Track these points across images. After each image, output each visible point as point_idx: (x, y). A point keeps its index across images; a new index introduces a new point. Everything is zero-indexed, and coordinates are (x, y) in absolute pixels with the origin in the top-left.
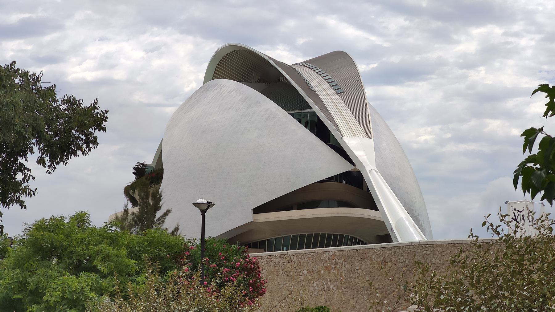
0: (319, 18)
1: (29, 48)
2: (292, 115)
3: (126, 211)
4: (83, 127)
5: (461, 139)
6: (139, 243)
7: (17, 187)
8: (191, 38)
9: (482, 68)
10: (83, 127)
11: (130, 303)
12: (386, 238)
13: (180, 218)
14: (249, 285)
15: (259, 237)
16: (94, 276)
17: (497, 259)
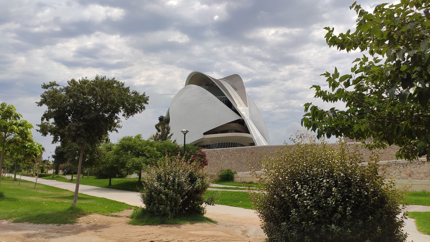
0: (229, 62)
1: (120, 73)
2: (218, 98)
3: (157, 134)
4: (139, 102)
5: (281, 107)
6: (161, 146)
7: (115, 125)
8: (181, 69)
9: (290, 81)
10: (139, 102)
11: (158, 168)
12: (253, 144)
13: (177, 138)
14: (202, 161)
15: (205, 144)
16: (144, 158)
17: (294, 152)
